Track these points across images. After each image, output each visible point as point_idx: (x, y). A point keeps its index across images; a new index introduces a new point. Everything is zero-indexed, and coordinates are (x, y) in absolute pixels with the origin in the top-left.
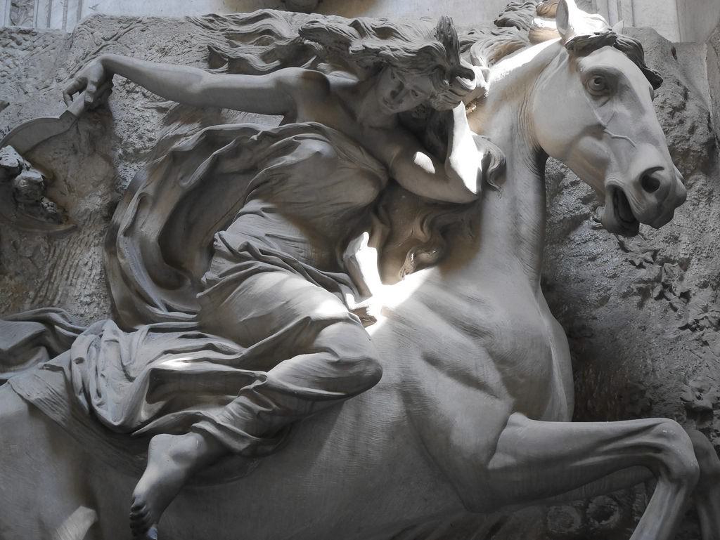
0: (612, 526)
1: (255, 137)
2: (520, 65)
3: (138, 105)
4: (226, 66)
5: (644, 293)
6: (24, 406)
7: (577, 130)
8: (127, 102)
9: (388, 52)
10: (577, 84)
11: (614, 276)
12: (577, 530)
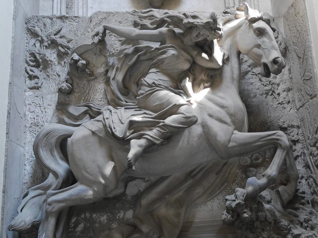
0: (260, 162)
1: (153, 49)
2: (233, 26)
3: (113, 39)
4: (139, 27)
5: (267, 94)
6: (90, 132)
7: (252, 46)
8: (110, 38)
11: (258, 89)
12: (249, 164)
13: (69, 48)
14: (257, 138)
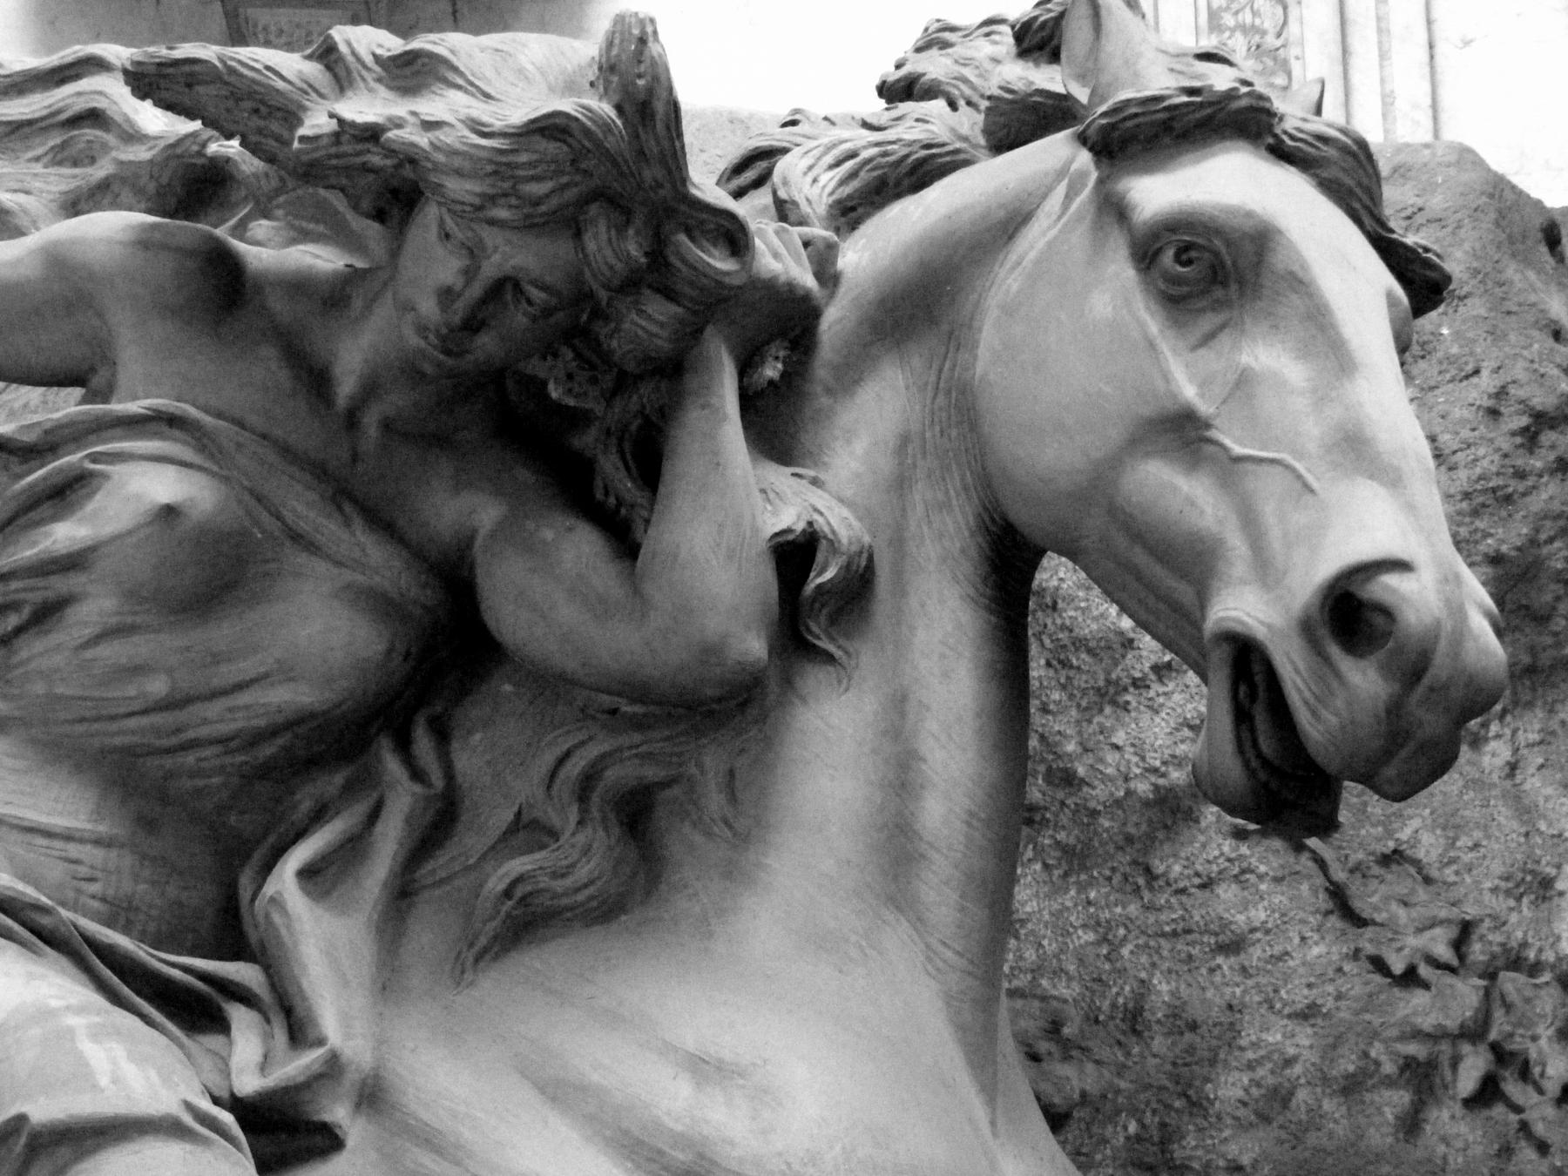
7: (1116, 434)
10: (1121, 270)
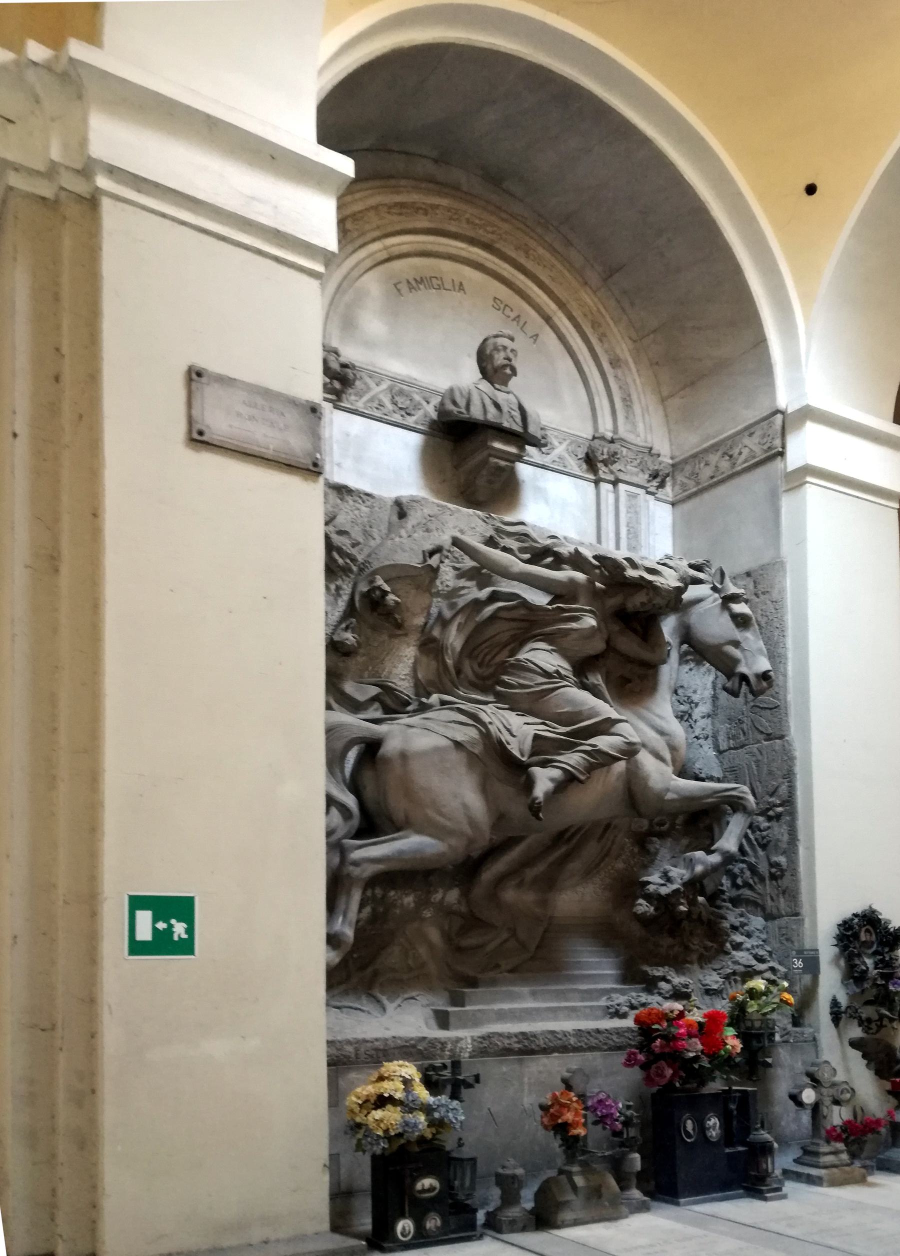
9: (658, 584)
13: (354, 560)
14: (710, 792)
